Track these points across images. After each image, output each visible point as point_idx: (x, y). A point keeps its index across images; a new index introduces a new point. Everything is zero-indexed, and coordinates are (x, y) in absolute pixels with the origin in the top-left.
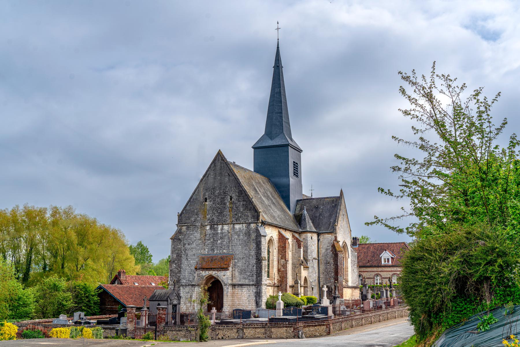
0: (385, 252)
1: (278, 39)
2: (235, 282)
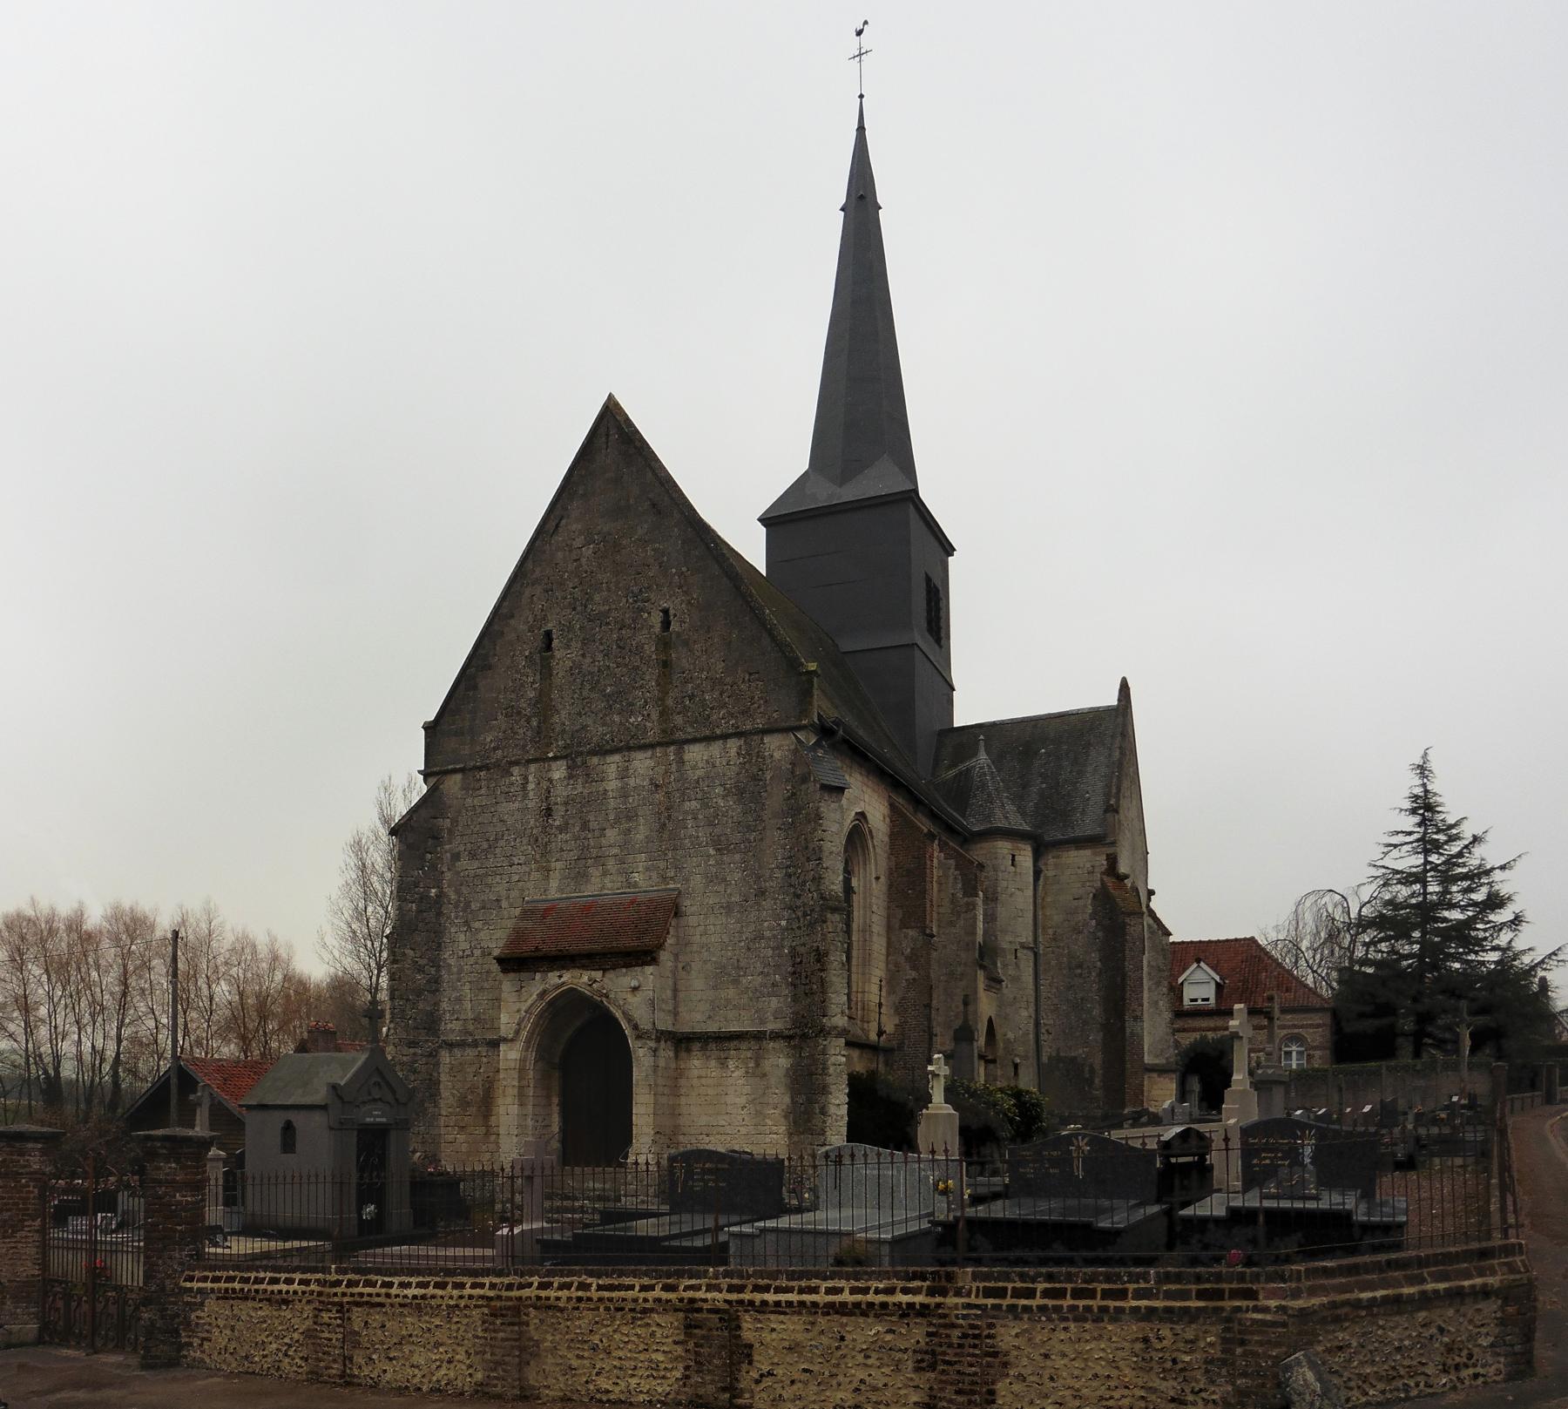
0: (1195, 965)
1: (861, 96)
2: (695, 1019)
